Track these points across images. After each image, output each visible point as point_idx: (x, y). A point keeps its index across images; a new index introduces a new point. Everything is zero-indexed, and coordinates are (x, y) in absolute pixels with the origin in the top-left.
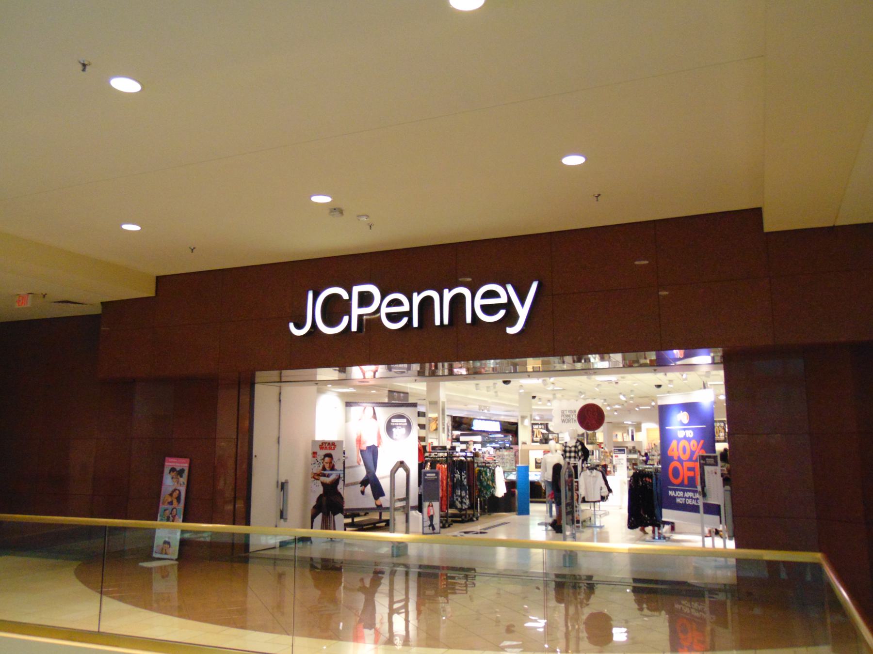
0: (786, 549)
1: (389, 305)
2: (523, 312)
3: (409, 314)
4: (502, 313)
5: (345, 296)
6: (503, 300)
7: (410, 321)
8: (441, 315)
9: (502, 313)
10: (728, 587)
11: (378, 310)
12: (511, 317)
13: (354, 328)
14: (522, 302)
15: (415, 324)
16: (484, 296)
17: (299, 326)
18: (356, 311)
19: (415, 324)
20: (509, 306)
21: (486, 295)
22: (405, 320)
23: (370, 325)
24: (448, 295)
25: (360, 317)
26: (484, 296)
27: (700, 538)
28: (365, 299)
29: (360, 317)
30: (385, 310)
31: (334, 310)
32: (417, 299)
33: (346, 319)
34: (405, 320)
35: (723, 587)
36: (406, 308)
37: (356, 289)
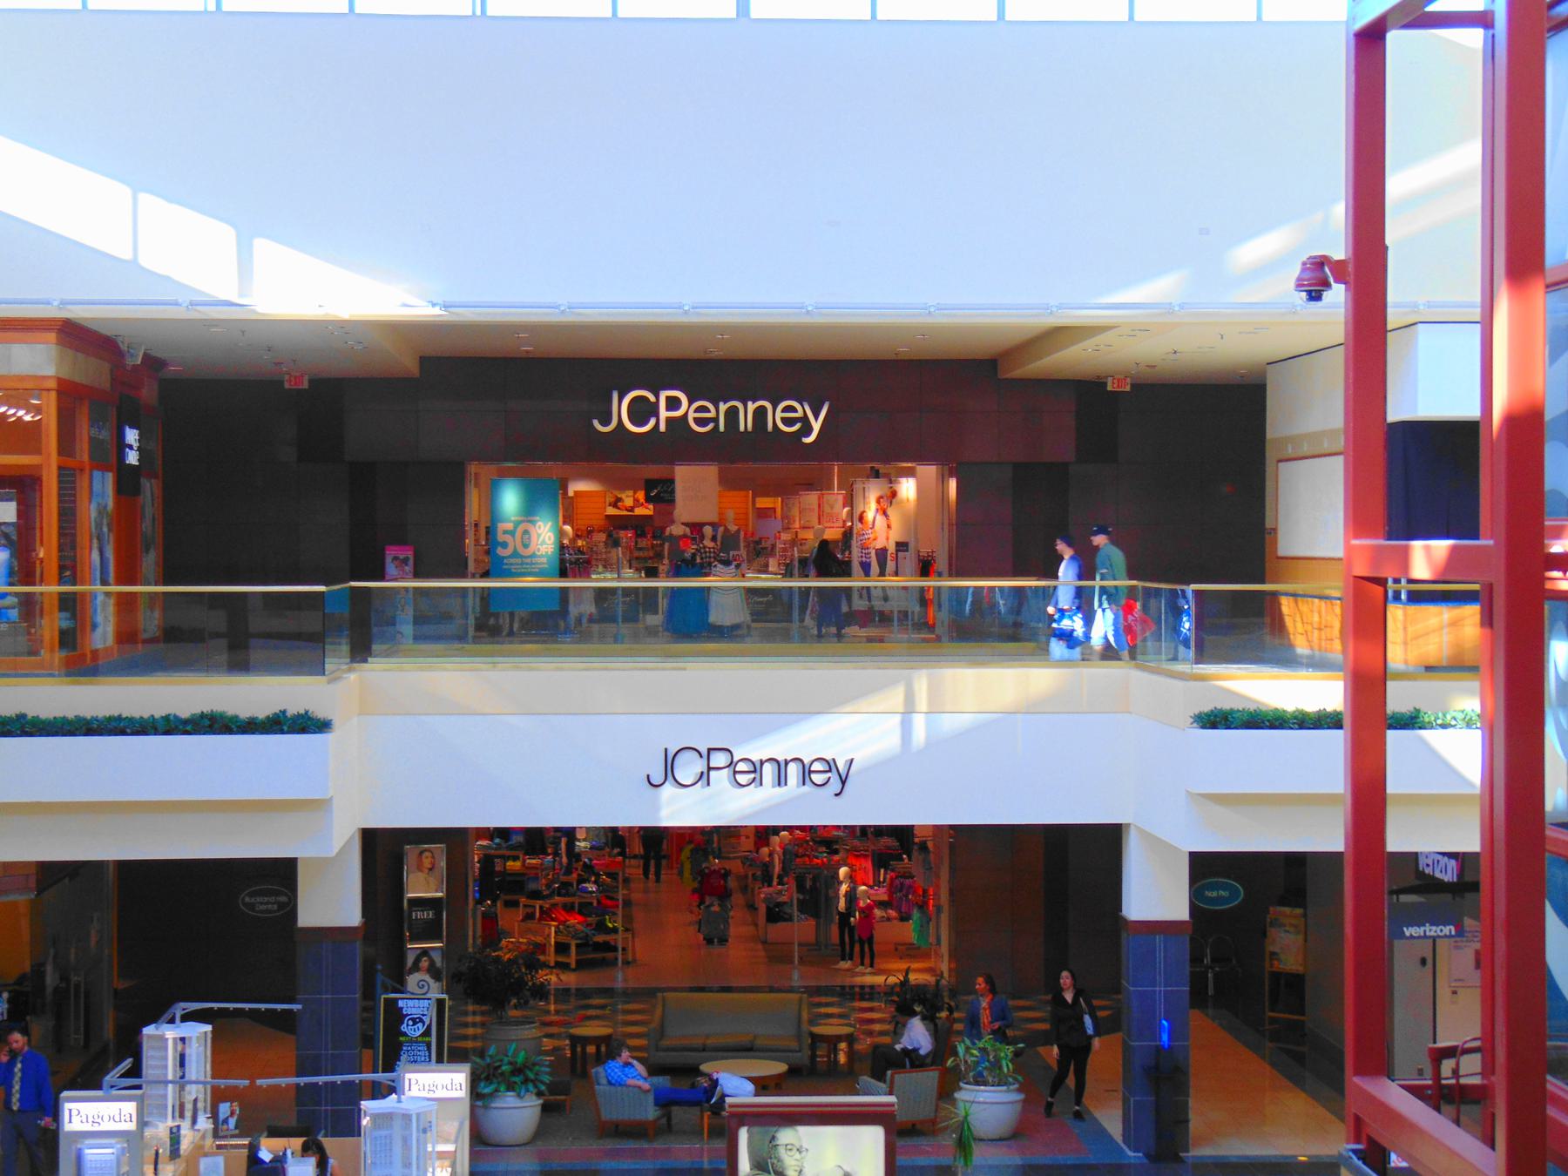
0: (1477, 477)
1: (697, 411)
2: (817, 427)
3: (716, 420)
4: (798, 426)
5: (652, 398)
6: (799, 414)
7: (717, 427)
8: (746, 422)
9: (798, 426)
10: (149, 393)
11: (686, 414)
12: (807, 429)
13: (662, 428)
14: (816, 418)
15: (722, 428)
16: (784, 410)
17: (606, 422)
18: (664, 414)
19: (722, 428)
20: (805, 419)
21: (786, 409)
22: (711, 426)
23: (677, 424)
24: (751, 407)
25: (669, 420)
26: (784, 410)
27: (924, 709)
28: (673, 404)
29: (669, 420)
30: (691, 415)
31: (642, 411)
32: (723, 407)
33: (652, 422)
34: (711, 426)
35: (853, 630)
36: (712, 414)
37: (664, 395)
